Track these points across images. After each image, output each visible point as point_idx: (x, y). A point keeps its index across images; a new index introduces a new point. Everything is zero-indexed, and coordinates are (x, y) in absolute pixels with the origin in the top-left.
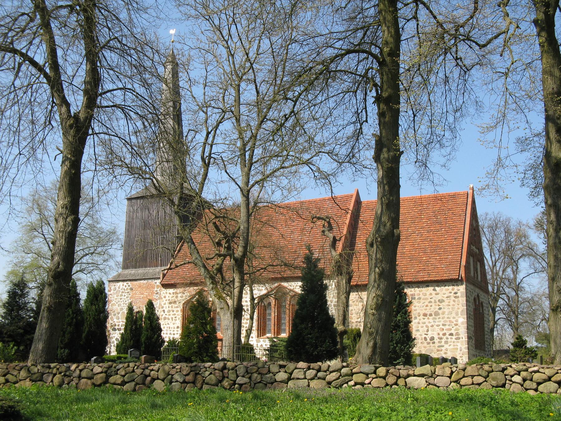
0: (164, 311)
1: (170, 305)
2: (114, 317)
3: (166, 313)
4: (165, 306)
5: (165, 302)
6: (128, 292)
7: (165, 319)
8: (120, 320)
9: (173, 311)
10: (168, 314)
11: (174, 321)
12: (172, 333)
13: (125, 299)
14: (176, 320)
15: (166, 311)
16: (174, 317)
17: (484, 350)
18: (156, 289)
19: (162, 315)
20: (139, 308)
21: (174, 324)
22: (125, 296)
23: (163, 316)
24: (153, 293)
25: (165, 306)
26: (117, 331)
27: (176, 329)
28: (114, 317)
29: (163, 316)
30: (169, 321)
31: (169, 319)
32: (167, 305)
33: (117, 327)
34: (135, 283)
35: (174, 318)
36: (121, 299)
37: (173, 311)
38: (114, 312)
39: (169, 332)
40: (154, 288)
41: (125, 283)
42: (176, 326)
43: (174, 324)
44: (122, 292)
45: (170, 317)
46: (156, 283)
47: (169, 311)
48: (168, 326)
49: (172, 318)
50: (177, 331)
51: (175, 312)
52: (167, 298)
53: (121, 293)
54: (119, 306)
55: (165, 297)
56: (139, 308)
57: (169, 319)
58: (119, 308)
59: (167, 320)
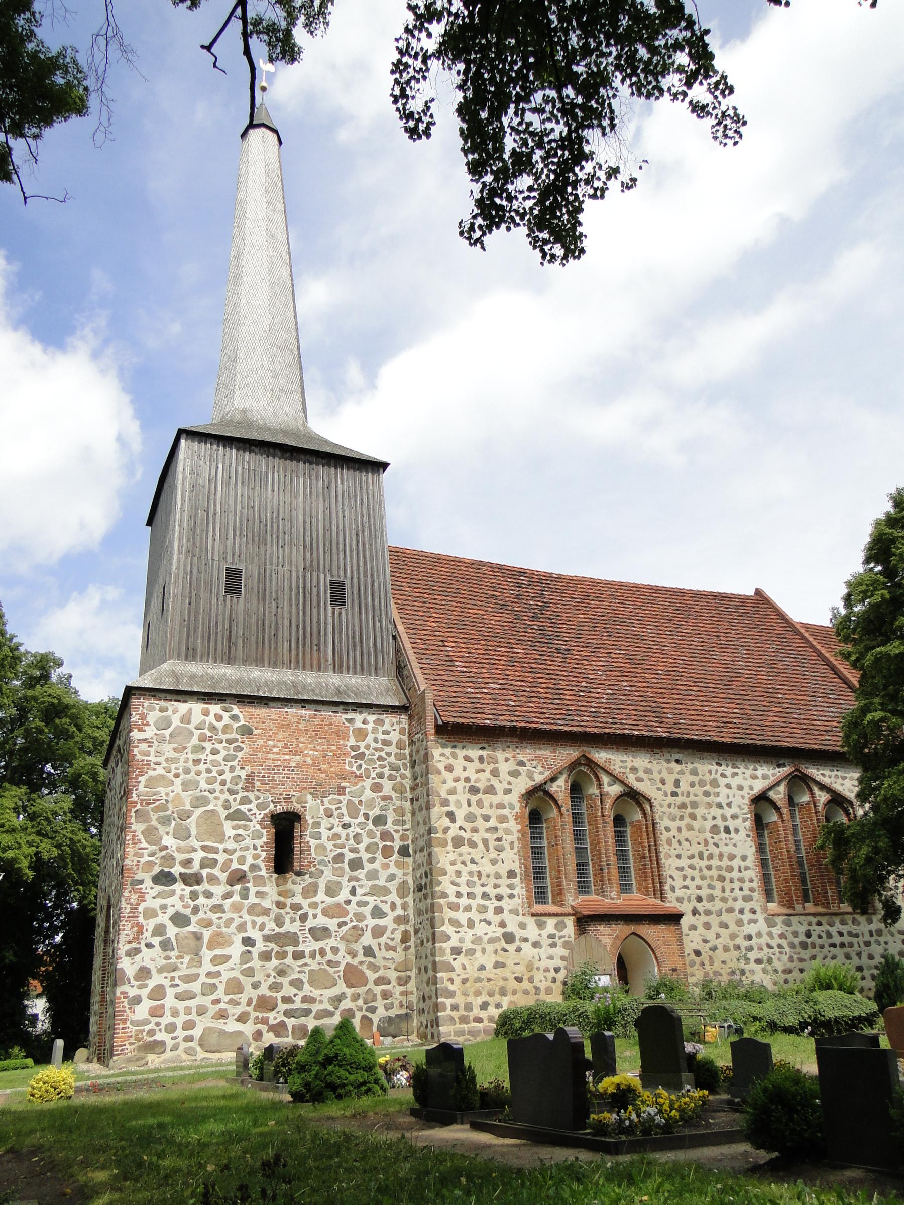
0: (451, 816)
1: (474, 799)
2: (162, 830)
3: (460, 822)
4: (452, 798)
5: (451, 784)
6: (230, 741)
7: (458, 842)
8: (193, 842)
9: (487, 818)
10: (468, 826)
11: (493, 854)
12: (492, 892)
13: (215, 763)
14: (500, 849)
15: (460, 815)
16: (491, 836)
17: (107, 1067)
18: (352, 741)
19: (446, 830)
20: (288, 799)
21: (494, 862)
22: (215, 752)
23: (451, 834)
24: (339, 754)
25: (452, 798)
26: (179, 886)
27: (504, 881)
28: (162, 830)
29: (451, 834)
30: (476, 853)
31: (473, 845)
32: (463, 797)
33: (177, 870)
34: (260, 712)
35: (492, 844)
36: (197, 762)
37: (487, 818)
38: (164, 808)
39: (478, 890)
40: (345, 737)
41: (215, 708)
42: (503, 869)
43: (494, 862)
44: (203, 738)
45: (476, 838)
46: (350, 721)
47: (470, 818)
48: (474, 868)
49: (485, 842)
50: (511, 886)
51: (493, 823)
52: (458, 772)
53: (195, 740)
54: (186, 786)
55: (450, 768)
56: (288, 799)
57: (473, 845)
58: (187, 798)
59: (465, 849)
